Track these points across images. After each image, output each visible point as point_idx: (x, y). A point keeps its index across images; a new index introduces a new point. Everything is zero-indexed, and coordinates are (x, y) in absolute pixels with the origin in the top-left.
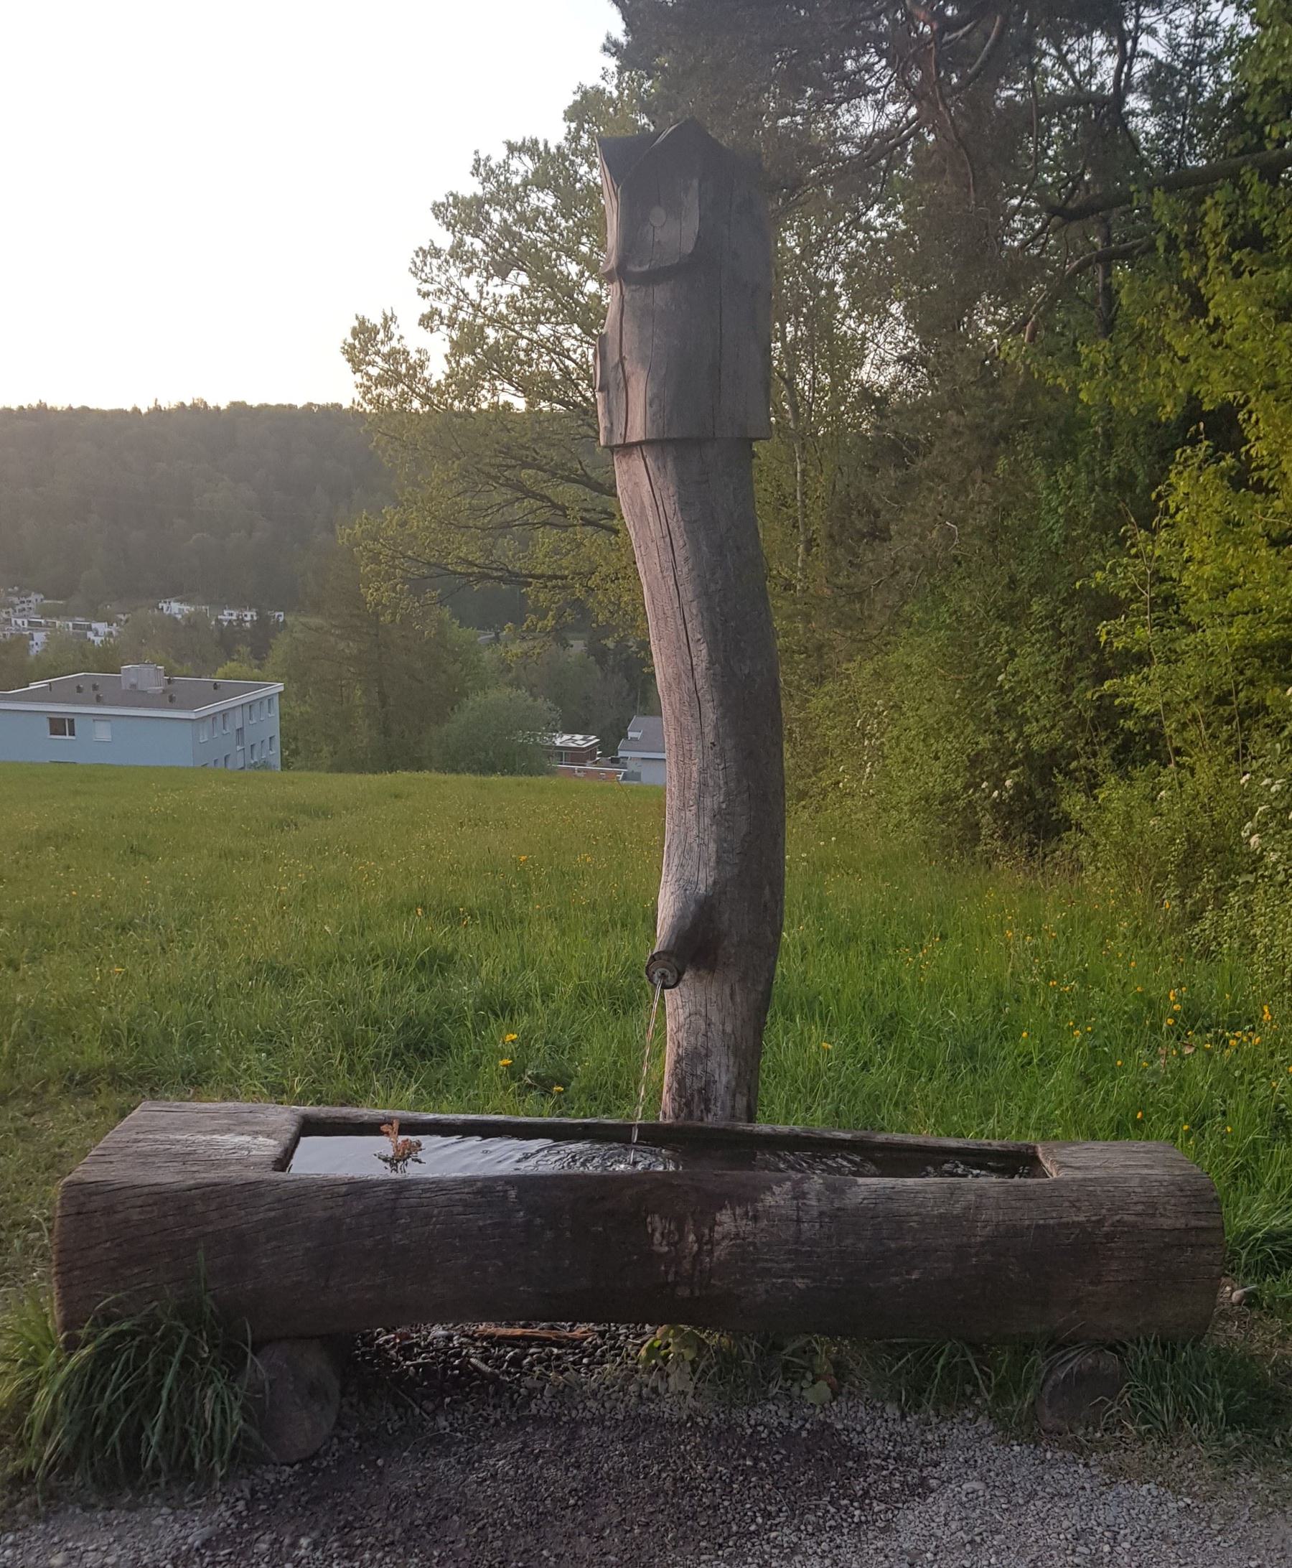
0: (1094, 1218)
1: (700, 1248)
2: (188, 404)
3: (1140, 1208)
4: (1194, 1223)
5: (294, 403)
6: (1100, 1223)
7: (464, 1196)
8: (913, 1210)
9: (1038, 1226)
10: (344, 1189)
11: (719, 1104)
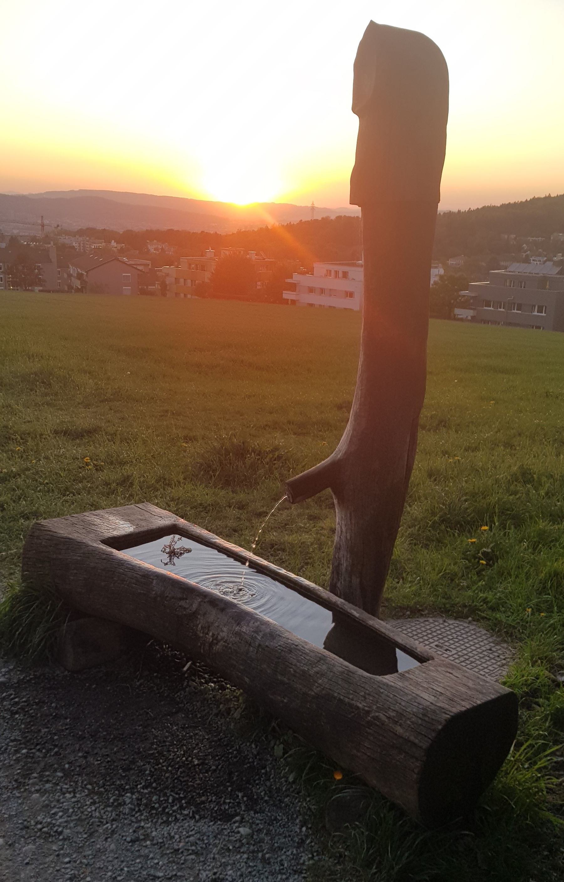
0: (366, 708)
1: (212, 641)
2: (528, 200)
3: (393, 714)
4: (412, 738)
5: (341, 215)
6: (368, 712)
7: (138, 576)
8: (295, 662)
9: (340, 700)
10: (104, 556)
11: (343, 577)
